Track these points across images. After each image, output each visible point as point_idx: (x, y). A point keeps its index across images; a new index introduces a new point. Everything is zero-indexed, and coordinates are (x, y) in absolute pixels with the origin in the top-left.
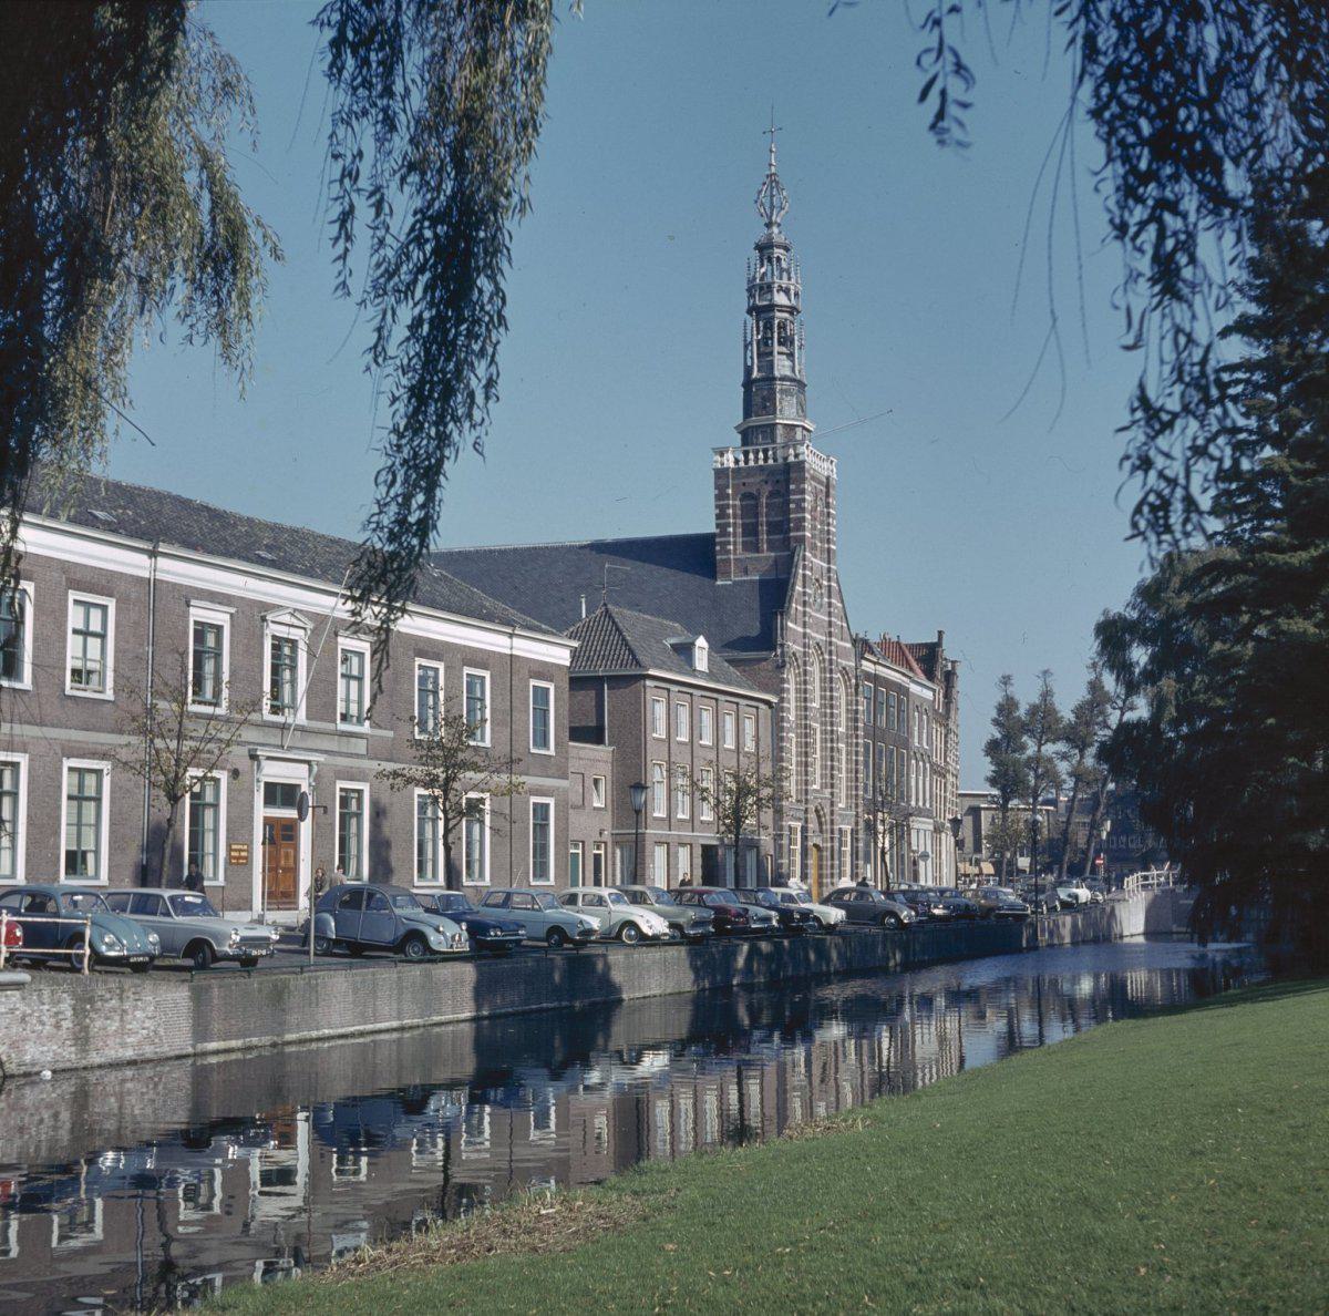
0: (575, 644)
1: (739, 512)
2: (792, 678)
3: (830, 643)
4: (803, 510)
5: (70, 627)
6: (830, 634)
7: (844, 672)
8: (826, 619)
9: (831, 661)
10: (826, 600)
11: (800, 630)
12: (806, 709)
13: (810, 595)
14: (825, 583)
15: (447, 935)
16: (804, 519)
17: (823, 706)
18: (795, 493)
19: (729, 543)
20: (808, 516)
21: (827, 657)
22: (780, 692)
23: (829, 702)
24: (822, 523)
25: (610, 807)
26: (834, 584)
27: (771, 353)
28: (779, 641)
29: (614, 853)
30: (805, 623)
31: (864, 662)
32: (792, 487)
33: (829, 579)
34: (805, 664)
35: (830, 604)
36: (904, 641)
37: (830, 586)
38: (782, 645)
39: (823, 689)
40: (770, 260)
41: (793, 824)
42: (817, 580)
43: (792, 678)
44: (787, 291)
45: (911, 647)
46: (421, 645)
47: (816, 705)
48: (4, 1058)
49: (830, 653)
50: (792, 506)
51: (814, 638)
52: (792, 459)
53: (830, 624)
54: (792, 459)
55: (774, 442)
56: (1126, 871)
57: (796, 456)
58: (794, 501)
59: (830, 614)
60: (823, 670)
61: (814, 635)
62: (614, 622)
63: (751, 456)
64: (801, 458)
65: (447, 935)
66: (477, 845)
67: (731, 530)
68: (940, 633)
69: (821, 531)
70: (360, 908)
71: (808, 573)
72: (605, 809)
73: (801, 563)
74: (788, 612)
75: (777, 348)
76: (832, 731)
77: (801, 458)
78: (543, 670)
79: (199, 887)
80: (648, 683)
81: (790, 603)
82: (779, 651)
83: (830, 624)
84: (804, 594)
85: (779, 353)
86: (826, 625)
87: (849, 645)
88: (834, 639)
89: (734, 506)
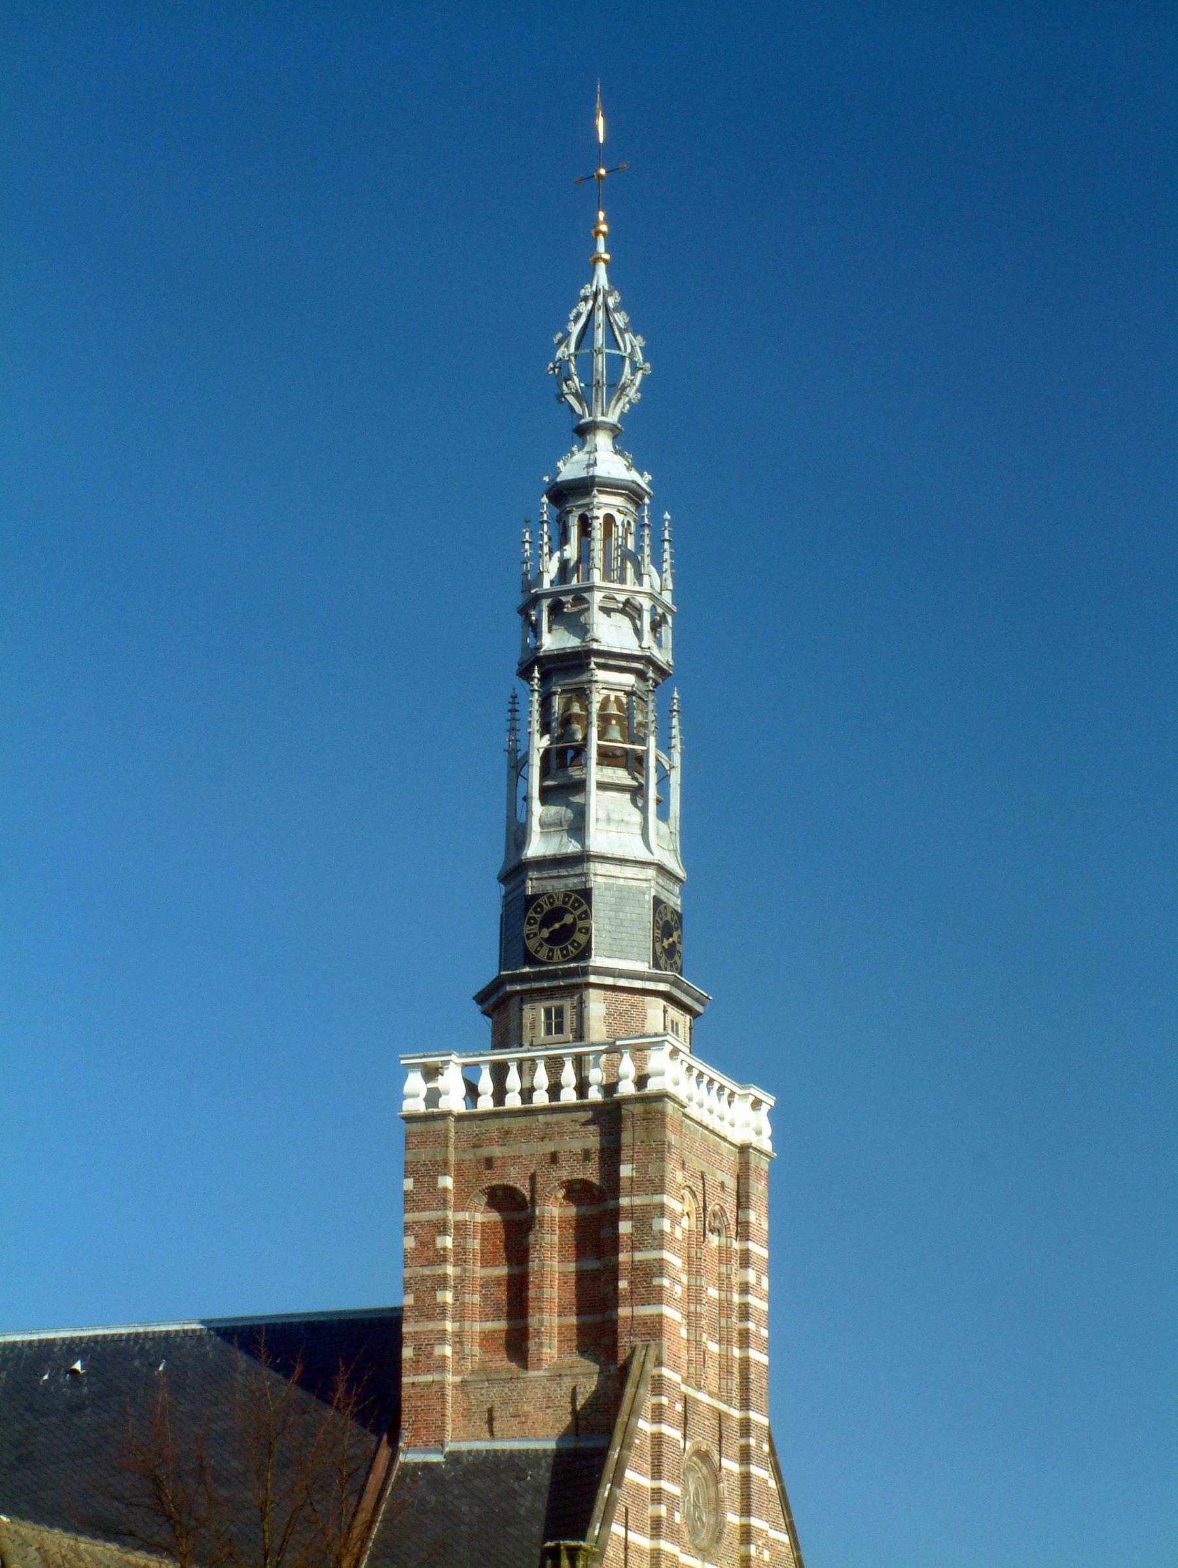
1: (475, 1244)
4: (660, 1240)
13: (673, 1499)
14: (731, 1466)
15: (280, 1501)
16: (659, 1268)
18: (636, 1186)
24: (724, 1283)
26: (760, 1472)
30: (657, 1523)
35: (747, 1535)
37: (746, 1478)
40: (585, 525)
48: (9, 1546)
50: (625, 1227)
52: (627, 1088)
55: (580, 1035)
56: (606, 763)
57: (641, 1081)
63: (513, 1081)
65: (280, 1501)
67: (448, 1297)
70: (552, 1034)
73: (650, 1401)
75: (596, 773)
77: (653, 1086)
81: (606, 1522)
85: (602, 786)
89: (460, 1227)
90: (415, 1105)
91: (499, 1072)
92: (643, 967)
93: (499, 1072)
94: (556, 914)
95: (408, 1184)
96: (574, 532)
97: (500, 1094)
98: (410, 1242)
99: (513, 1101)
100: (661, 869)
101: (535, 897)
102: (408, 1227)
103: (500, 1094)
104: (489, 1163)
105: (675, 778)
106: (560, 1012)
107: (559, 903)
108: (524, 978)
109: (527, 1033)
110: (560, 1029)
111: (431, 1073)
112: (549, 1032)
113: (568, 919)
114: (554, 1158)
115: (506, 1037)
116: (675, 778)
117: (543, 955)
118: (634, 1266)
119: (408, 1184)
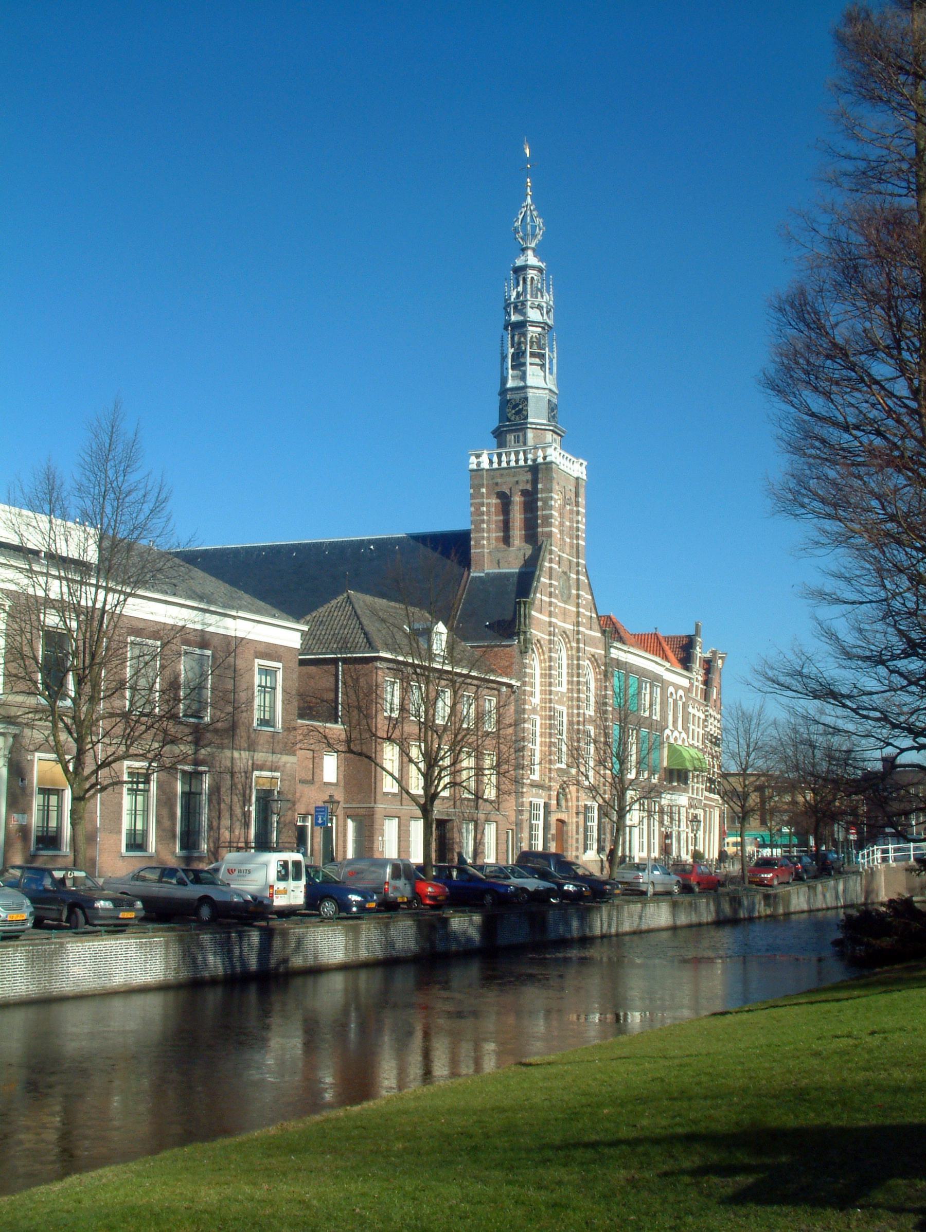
0: (305, 628)
1: (493, 509)
2: (536, 663)
3: (578, 632)
4: (551, 507)
5: (281, 670)
6: (578, 624)
7: (594, 659)
8: (575, 609)
9: (578, 650)
10: (574, 592)
11: (547, 619)
12: (550, 693)
14: (573, 576)
16: (551, 516)
17: (570, 690)
19: (483, 538)
20: (555, 513)
21: (574, 645)
22: (521, 676)
23: (576, 685)
24: (571, 521)
25: (342, 784)
27: (524, 364)
28: (522, 627)
29: (345, 825)
31: (612, 650)
32: (540, 486)
33: (578, 573)
34: (550, 650)
35: (578, 596)
36: (662, 633)
37: (578, 580)
38: (525, 633)
39: (570, 675)
41: (535, 800)
42: (565, 573)
43: (536, 663)
44: (539, 307)
45: (668, 639)
46: (136, 624)
47: (564, 688)
49: (578, 641)
50: (540, 504)
51: (559, 627)
52: (540, 460)
53: (578, 614)
54: (540, 460)
55: (525, 444)
57: (545, 458)
58: (542, 500)
59: (578, 605)
60: (570, 658)
61: (560, 624)
62: (353, 608)
63: (504, 458)
64: (548, 459)
66: (628, 843)
68: (697, 625)
69: (571, 528)
71: (555, 566)
72: (336, 785)
73: (548, 557)
74: (533, 603)
75: (529, 360)
76: (578, 715)
77: (548, 459)
78: (271, 652)
79: (465, 877)
80: (378, 664)
82: (522, 638)
83: (578, 614)
84: (551, 585)
85: (531, 364)
86: (574, 615)
87: (599, 635)
88: (581, 629)
89: (488, 505)
90: (474, 467)
91: (499, 456)
92: (545, 422)
93: (499, 456)
94: (517, 405)
95: (472, 491)
96: (521, 282)
97: (500, 462)
98: (472, 509)
99: (504, 465)
100: (550, 390)
101: (510, 400)
102: (471, 505)
103: (500, 462)
104: (497, 484)
105: (555, 361)
106: (518, 436)
107: (518, 402)
108: (507, 426)
109: (508, 444)
110: (518, 442)
111: (478, 456)
112: (515, 442)
113: (521, 407)
114: (517, 482)
115: (501, 444)
116: (555, 361)
117: (513, 418)
118: (543, 516)
119: (472, 491)
